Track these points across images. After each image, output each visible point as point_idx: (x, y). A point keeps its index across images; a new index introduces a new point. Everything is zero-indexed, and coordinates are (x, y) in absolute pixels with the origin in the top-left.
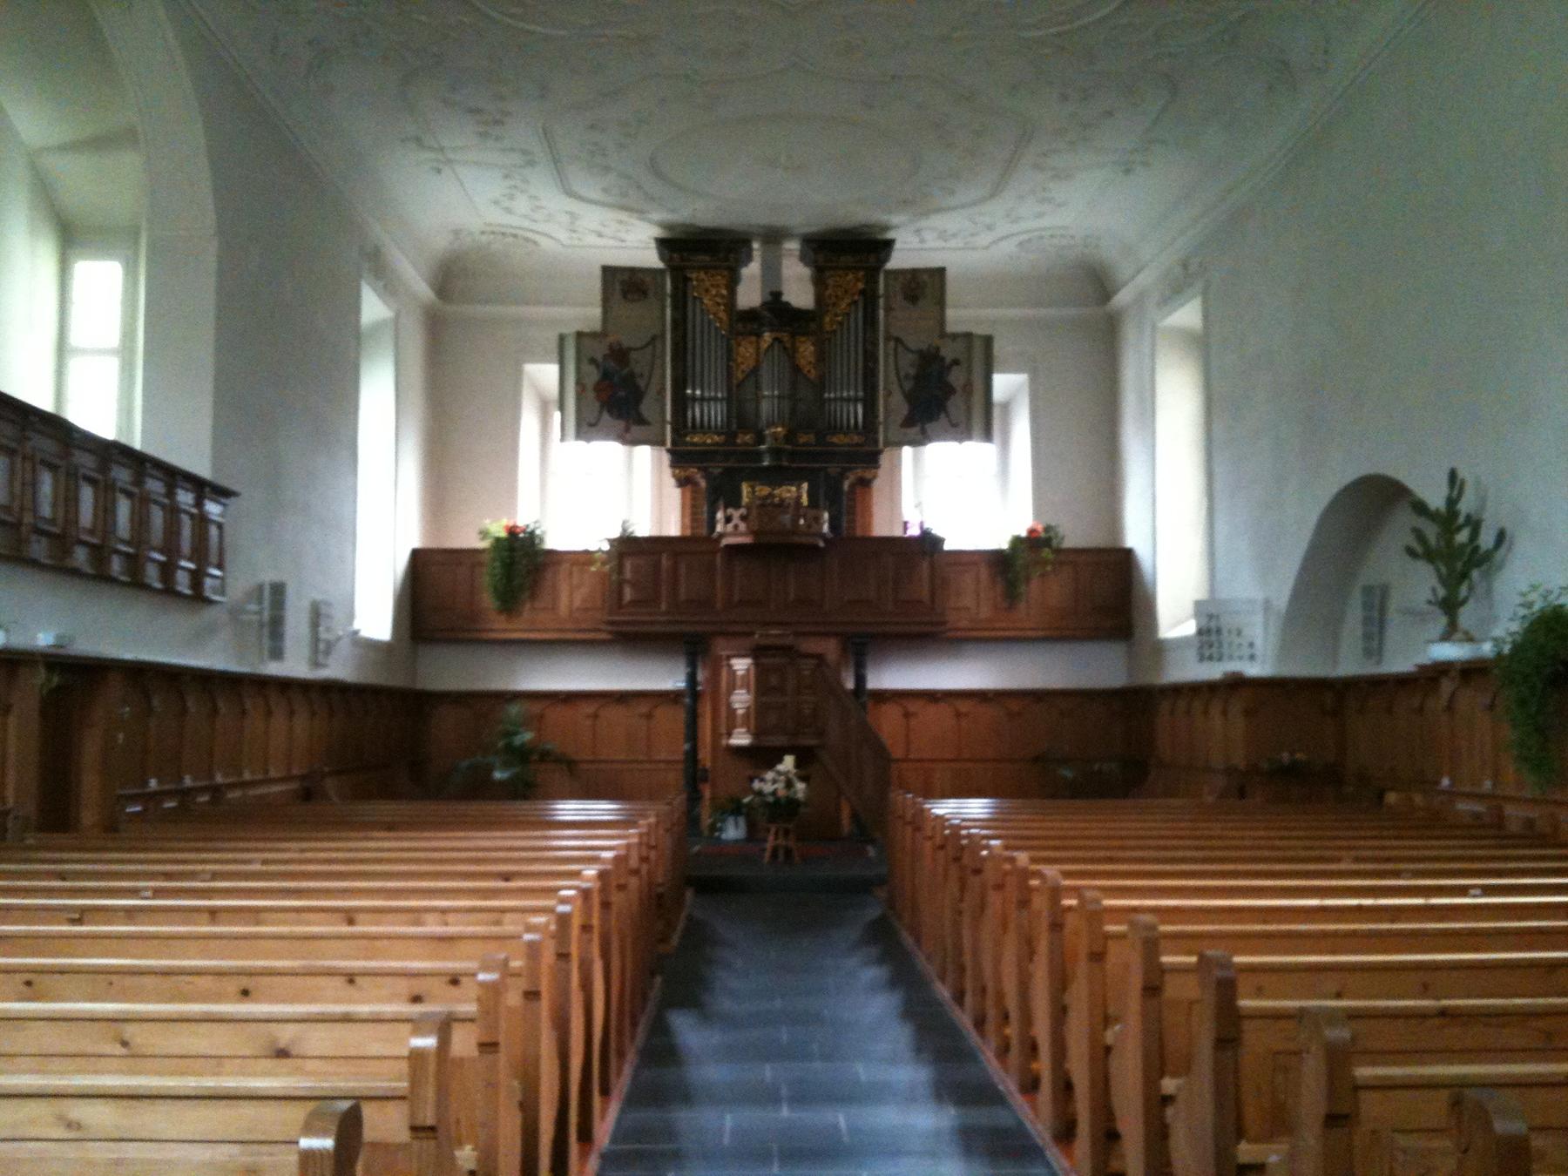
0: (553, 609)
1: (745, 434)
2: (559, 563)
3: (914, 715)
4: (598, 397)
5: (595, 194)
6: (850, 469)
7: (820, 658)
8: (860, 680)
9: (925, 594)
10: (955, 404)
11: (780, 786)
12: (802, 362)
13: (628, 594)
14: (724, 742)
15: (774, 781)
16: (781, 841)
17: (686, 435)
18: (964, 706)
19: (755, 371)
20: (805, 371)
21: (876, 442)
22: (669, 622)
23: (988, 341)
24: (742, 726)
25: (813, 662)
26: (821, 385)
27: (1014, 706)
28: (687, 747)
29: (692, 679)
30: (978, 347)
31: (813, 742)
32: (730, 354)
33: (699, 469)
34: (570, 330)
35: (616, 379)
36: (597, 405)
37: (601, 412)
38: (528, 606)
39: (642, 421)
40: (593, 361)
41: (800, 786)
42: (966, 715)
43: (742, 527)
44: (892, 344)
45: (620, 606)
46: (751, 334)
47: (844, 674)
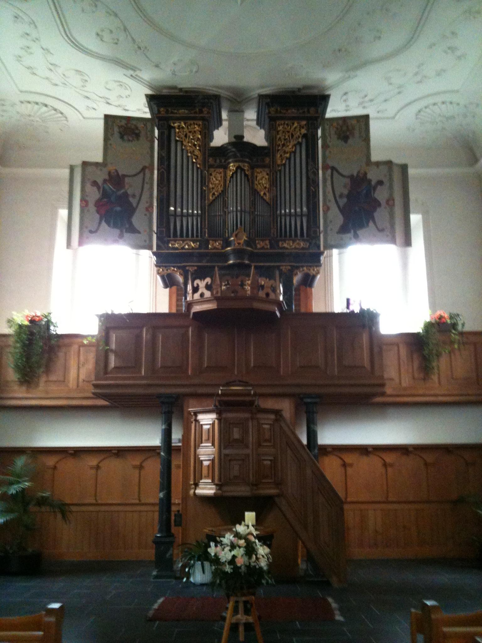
0: (64, 381)
1: (216, 241)
2: (69, 345)
3: (351, 465)
4: (98, 212)
5: (92, 44)
6: (298, 268)
7: (278, 413)
8: (312, 435)
9: (366, 363)
10: (381, 214)
11: (239, 552)
12: (259, 188)
13: (112, 362)
14: (192, 492)
15: (233, 546)
16: (241, 617)
17: (168, 242)
18: (390, 458)
19: (224, 192)
20: (262, 193)
21: (319, 247)
22: (149, 386)
23: (404, 168)
24: (207, 477)
25: (273, 417)
26: (273, 205)
27: (430, 458)
28: (161, 495)
29: (167, 435)
30: (397, 175)
31: (273, 491)
32: (204, 181)
33: (179, 268)
34: (78, 162)
35: (113, 199)
36: (97, 216)
37: (100, 223)
38: (43, 379)
39: (133, 230)
40: (95, 183)
41: (262, 550)
42: (391, 465)
43: (208, 294)
44: (329, 171)
45: (106, 373)
46: (219, 167)
47: (298, 432)
